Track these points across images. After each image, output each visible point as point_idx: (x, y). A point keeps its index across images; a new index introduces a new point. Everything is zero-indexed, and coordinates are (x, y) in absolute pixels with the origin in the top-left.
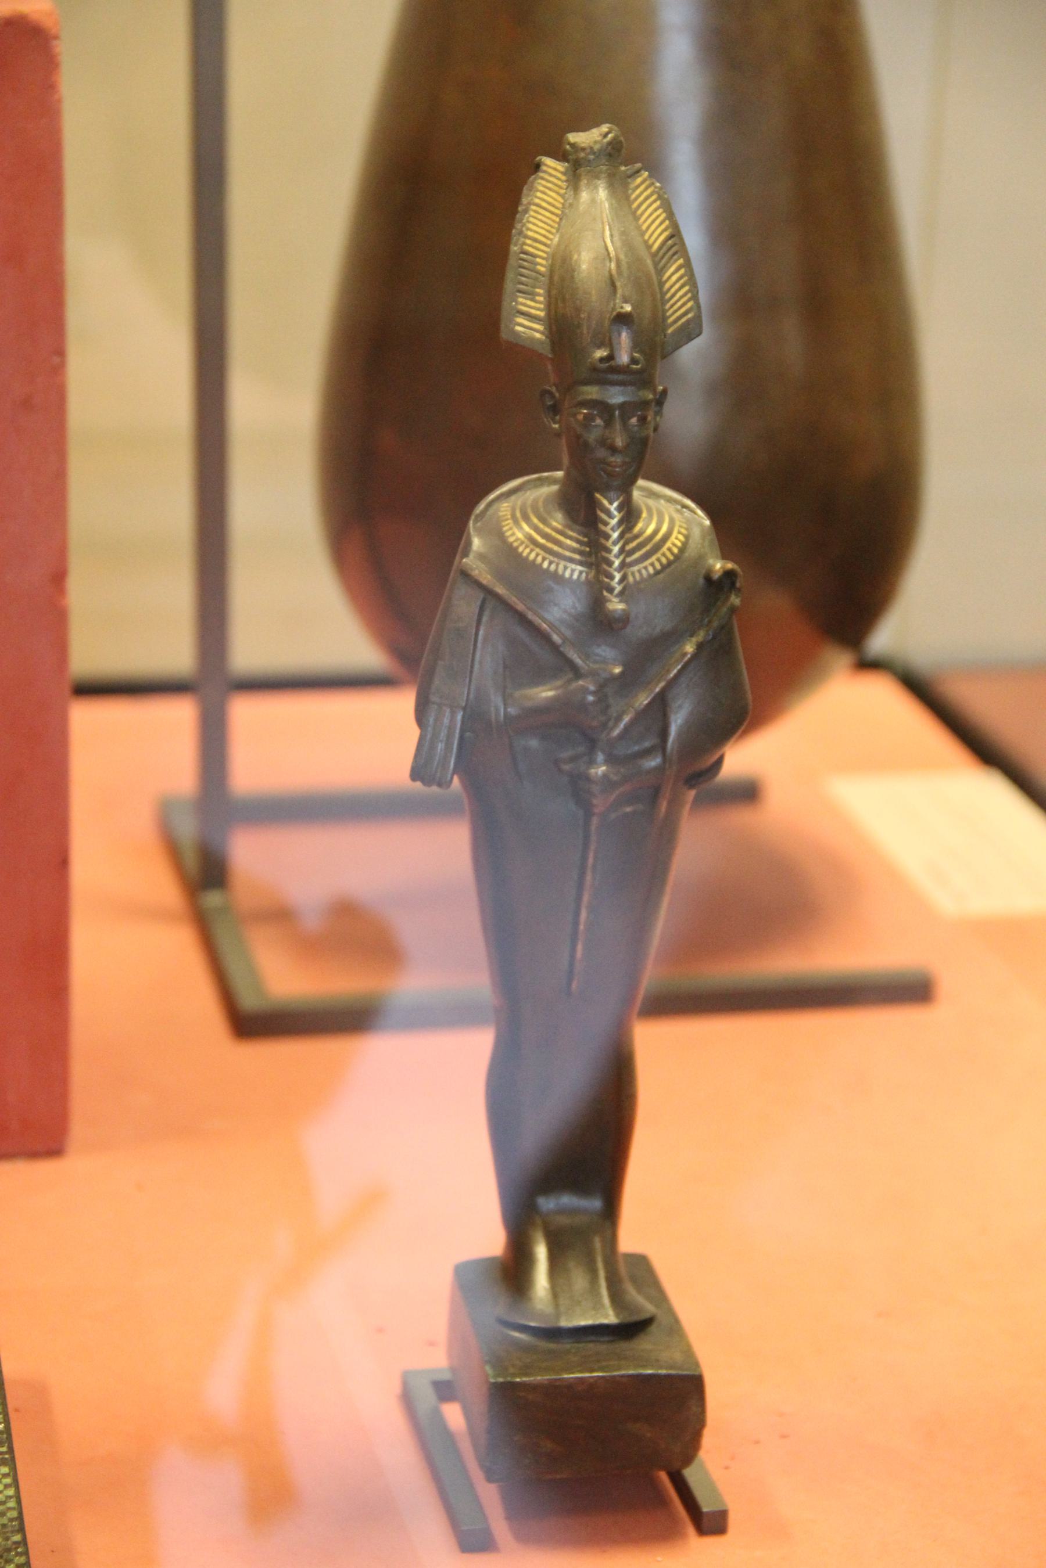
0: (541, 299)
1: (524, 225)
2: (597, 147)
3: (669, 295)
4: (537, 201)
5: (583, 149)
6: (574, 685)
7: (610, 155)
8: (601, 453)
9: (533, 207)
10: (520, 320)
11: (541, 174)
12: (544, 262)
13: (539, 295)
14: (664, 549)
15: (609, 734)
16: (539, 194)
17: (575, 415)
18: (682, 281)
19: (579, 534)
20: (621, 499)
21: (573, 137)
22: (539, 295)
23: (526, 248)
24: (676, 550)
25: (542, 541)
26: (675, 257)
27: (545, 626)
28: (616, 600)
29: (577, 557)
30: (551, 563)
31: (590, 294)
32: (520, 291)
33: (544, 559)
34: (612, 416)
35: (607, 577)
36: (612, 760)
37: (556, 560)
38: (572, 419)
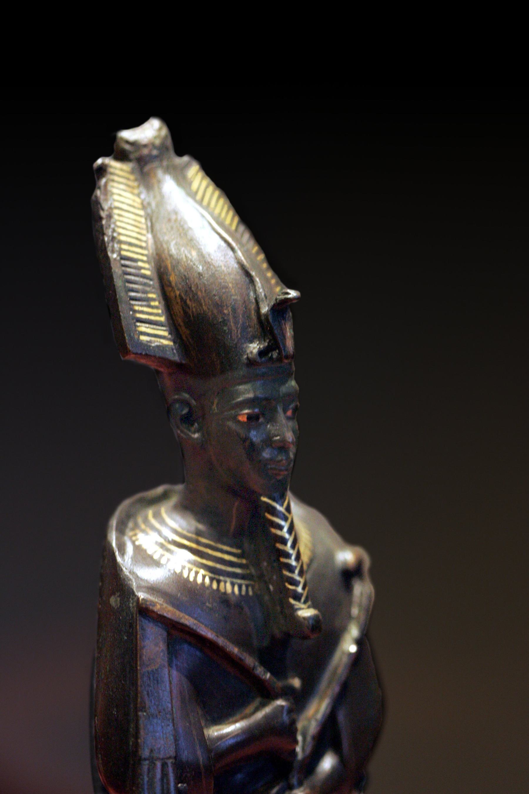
1: (114, 231)
2: (158, 142)
5: (145, 146)
9: (116, 211)
10: (143, 328)
11: (112, 177)
12: (146, 266)
13: (153, 300)
21: (127, 135)
22: (153, 300)
23: (124, 253)
25: (223, 568)
31: (227, 288)
35: (291, 584)
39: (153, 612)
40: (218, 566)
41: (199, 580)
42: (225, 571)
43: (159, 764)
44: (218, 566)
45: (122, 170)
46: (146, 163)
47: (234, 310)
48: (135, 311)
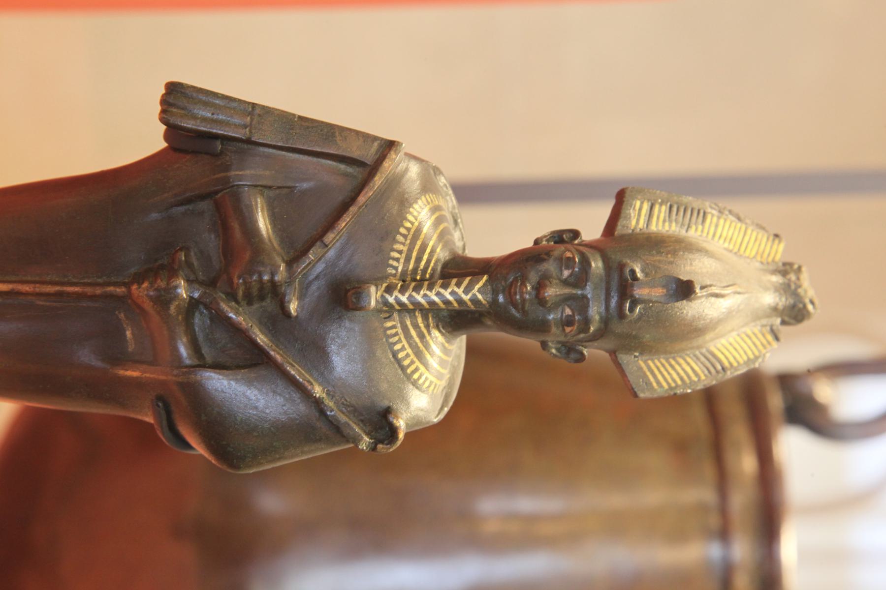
0: (667, 228)
3: (673, 362)
4: (749, 232)
6: (278, 260)
7: (794, 306)
8: (533, 277)
10: (646, 207)
13: (670, 226)
14: (417, 363)
15: (223, 300)
16: (754, 234)
18: (685, 378)
20: (484, 302)
24: (416, 376)
26: (706, 372)
27: (343, 225)
28: (379, 293)
29: (411, 267)
30: (405, 236)
32: (671, 207)
33: (408, 229)
34: (575, 285)
36: (193, 305)
37: (408, 242)
39: (390, 150)
41: (397, 246)
42: (415, 244)
45: (777, 251)
47: (671, 263)
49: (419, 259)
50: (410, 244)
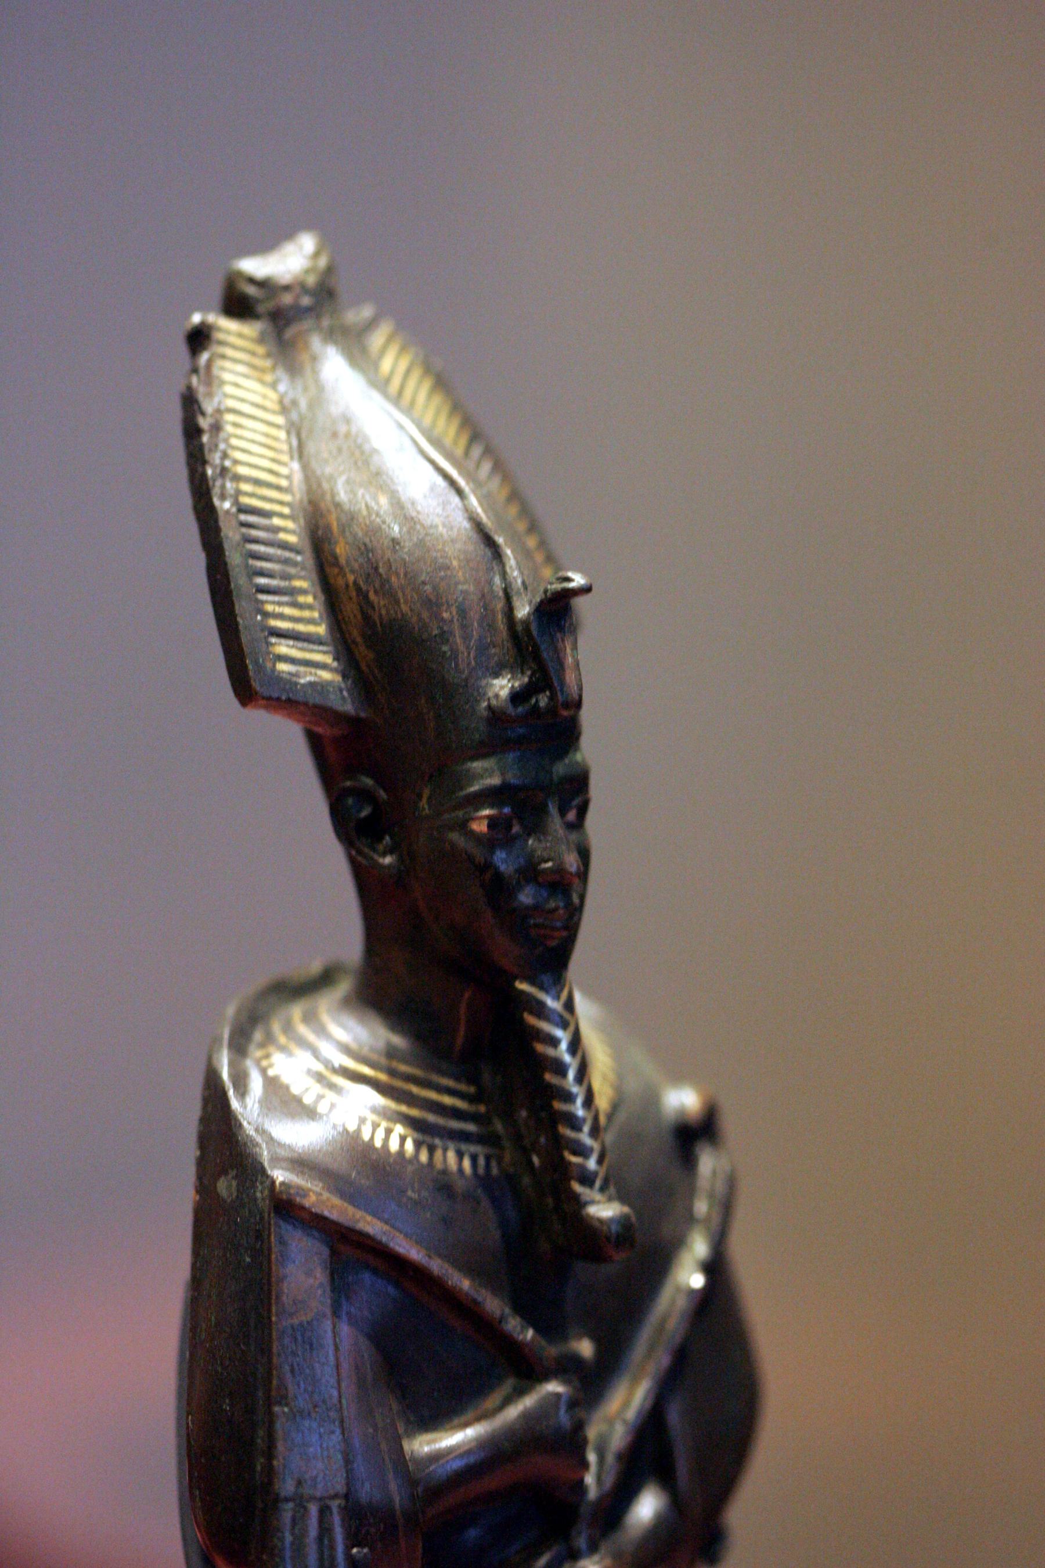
0: (309, 599)
1: (225, 456)
5: (287, 288)
9: (229, 417)
10: (283, 648)
12: (290, 524)
17: (463, 826)
19: (457, 1079)
23: (245, 500)
29: (471, 1127)
35: (575, 1153)
38: (454, 836)
39: (302, 1208)
40: (431, 1118)
43: (313, 1509)
44: (431, 1118)
45: (240, 335)
46: (288, 323)
47: (463, 613)
48: (266, 615)
49: (455, 1113)
50: (442, 1137)
